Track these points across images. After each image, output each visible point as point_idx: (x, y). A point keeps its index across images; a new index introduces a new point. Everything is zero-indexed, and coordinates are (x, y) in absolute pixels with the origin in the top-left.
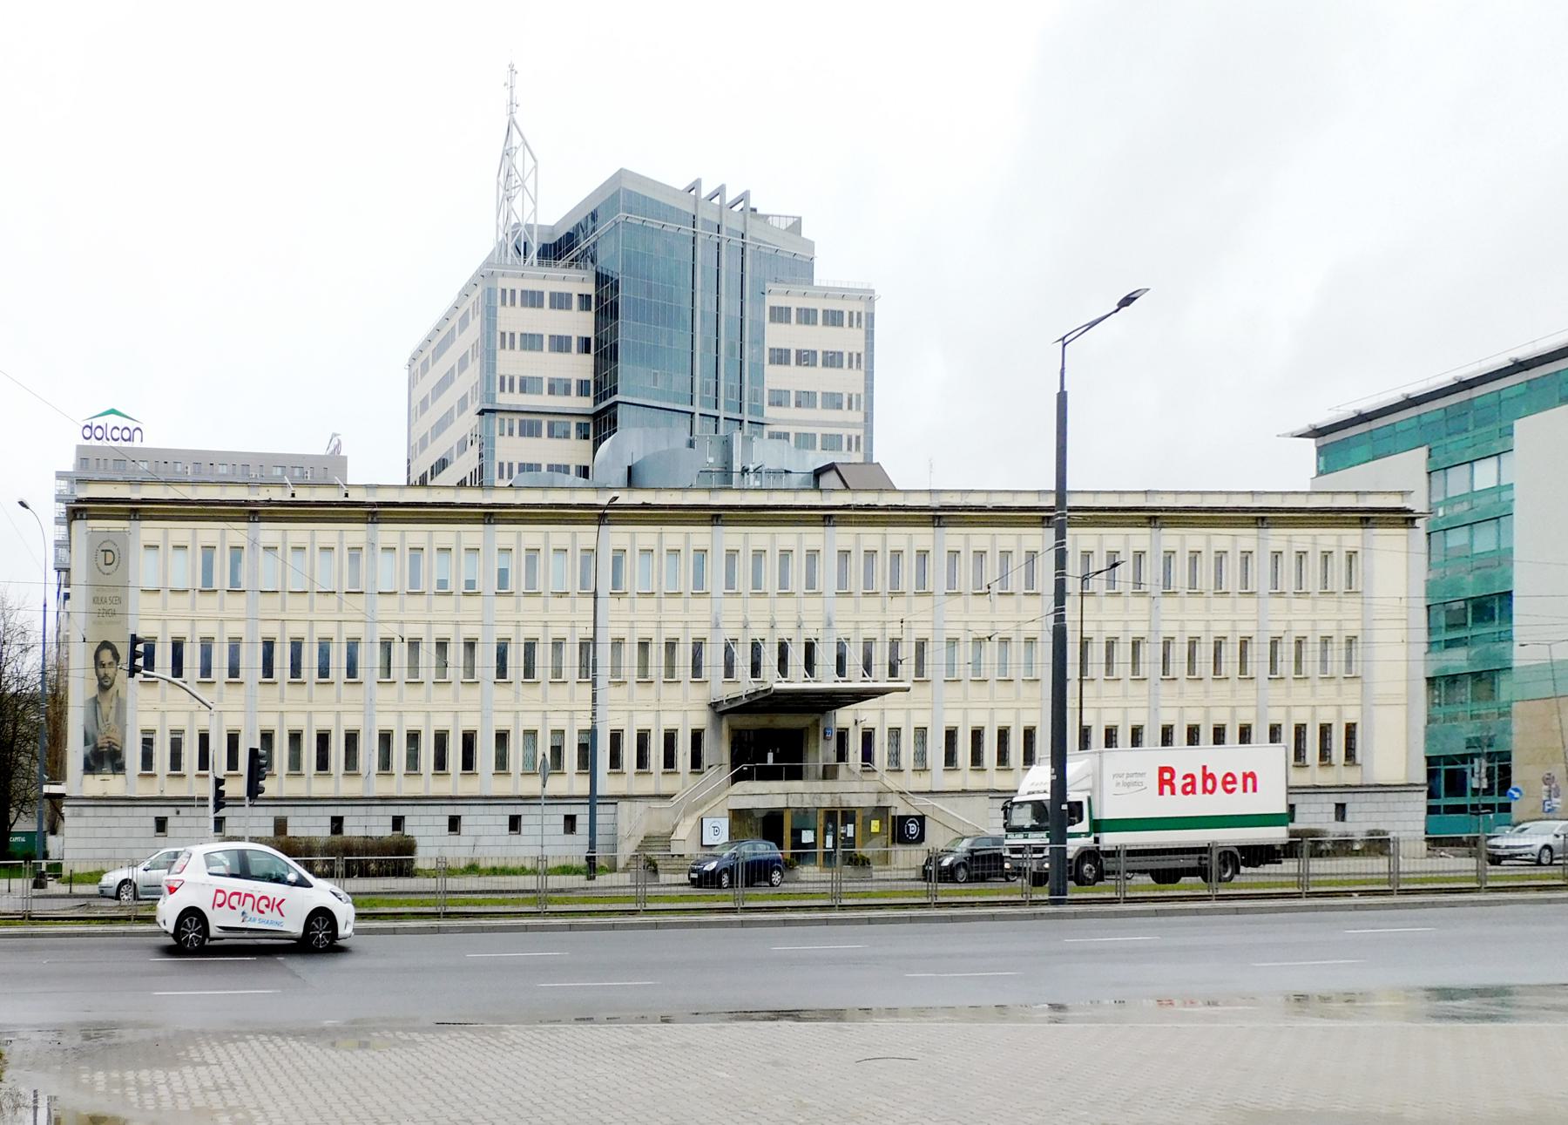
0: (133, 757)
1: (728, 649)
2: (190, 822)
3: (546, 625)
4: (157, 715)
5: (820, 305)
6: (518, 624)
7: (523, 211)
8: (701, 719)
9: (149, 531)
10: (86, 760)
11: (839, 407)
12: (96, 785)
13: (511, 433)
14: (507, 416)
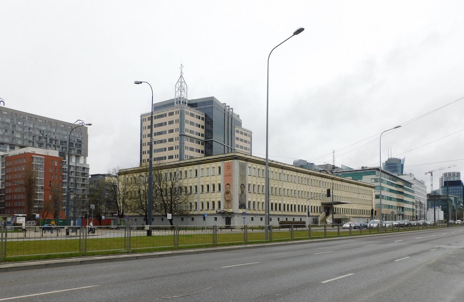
1: (196, 175)
3: (261, 183)
5: (240, 130)
6: (261, 183)
7: (184, 95)
8: (320, 205)
9: (249, 164)
12: (241, 211)
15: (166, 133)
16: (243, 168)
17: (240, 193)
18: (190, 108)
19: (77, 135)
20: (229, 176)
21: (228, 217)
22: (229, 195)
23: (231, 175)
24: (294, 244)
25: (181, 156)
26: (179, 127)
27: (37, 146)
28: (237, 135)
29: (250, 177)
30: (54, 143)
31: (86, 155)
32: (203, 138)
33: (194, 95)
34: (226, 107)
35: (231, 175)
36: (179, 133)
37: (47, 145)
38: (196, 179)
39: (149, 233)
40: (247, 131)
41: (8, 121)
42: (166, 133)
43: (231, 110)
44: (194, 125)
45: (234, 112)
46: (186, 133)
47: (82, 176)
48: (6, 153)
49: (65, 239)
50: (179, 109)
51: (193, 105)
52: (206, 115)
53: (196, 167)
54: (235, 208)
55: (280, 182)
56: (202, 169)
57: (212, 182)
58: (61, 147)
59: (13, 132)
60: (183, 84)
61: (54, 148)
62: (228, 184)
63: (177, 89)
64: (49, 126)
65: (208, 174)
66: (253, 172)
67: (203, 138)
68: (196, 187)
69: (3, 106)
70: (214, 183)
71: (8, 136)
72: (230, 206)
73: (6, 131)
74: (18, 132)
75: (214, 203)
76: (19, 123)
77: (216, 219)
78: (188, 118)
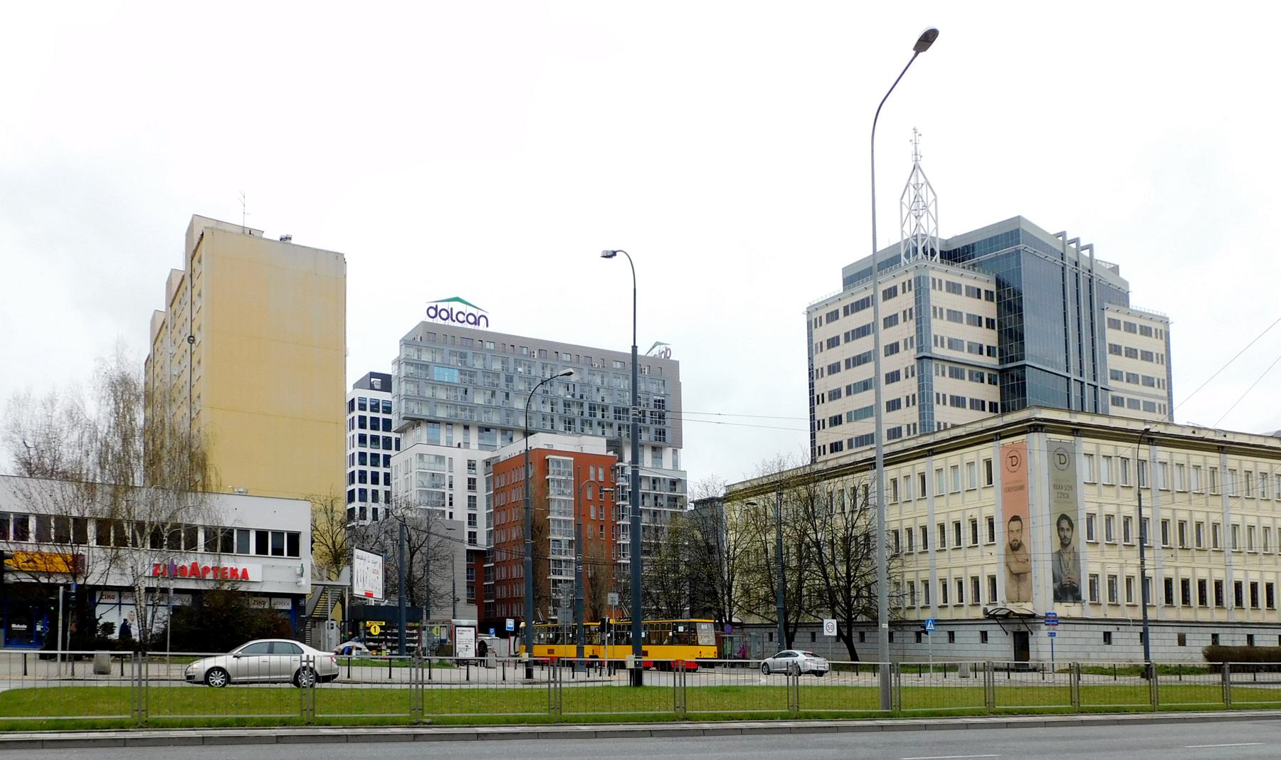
0: (1085, 593)
2: (1126, 635)
4: (1098, 566)
5: (1123, 318)
7: (927, 226)
9: (1087, 444)
10: (1055, 592)
11: (1153, 385)
12: (1062, 610)
13: (943, 374)
14: (940, 363)
15: (847, 361)
16: (1062, 459)
17: (1057, 547)
18: (950, 268)
19: (653, 388)
20: (1017, 489)
21: (1021, 630)
22: (1020, 555)
23: (1022, 488)
24: (1083, 723)
25: (926, 423)
26: (913, 333)
27: (561, 427)
28: (1113, 336)
29: (1093, 489)
30: (599, 415)
31: (677, 445)
32: (993, 362)
33: (953, 226)
34: (1066, 243)
35: (1022, 488)
36: (914, 351)
37: (583, 424)
38: (924, 504)
39: (636, 677)
40: (1152, 318)
41: (497, 366)
42: (847, 361)
43: (1086, 253)
44: (960, 318)
45: (1096, 256)
46: (938, 351)
47: (669, 506)
48: (495, 454)
49: (519, 686)
50: (911, 276)
51: (955, 255)
52: (1000, 283)
53: (921, 465)
54: (1041, 600)
55: (1217, 501)
56: (939, 470)
57: (969, 513)
58: (616, 427)
59: (507, 395)
60: (923, 191)
61: (600, 431)
62: (1016, 518)
63: (906, 211)
64: (586, 370)
65: (972, 482)
66: (1105, 472)
67: (993, 362)
68: (924, 529)
69: (485, 329)
70: (976, 514)
71: (498, 408)
72: (1023, 594)
73: (493, 394)
74: (519, 393)
75: (976, 581)
76: (520, 369)
77: (984, 636)
78: (940, 298)
